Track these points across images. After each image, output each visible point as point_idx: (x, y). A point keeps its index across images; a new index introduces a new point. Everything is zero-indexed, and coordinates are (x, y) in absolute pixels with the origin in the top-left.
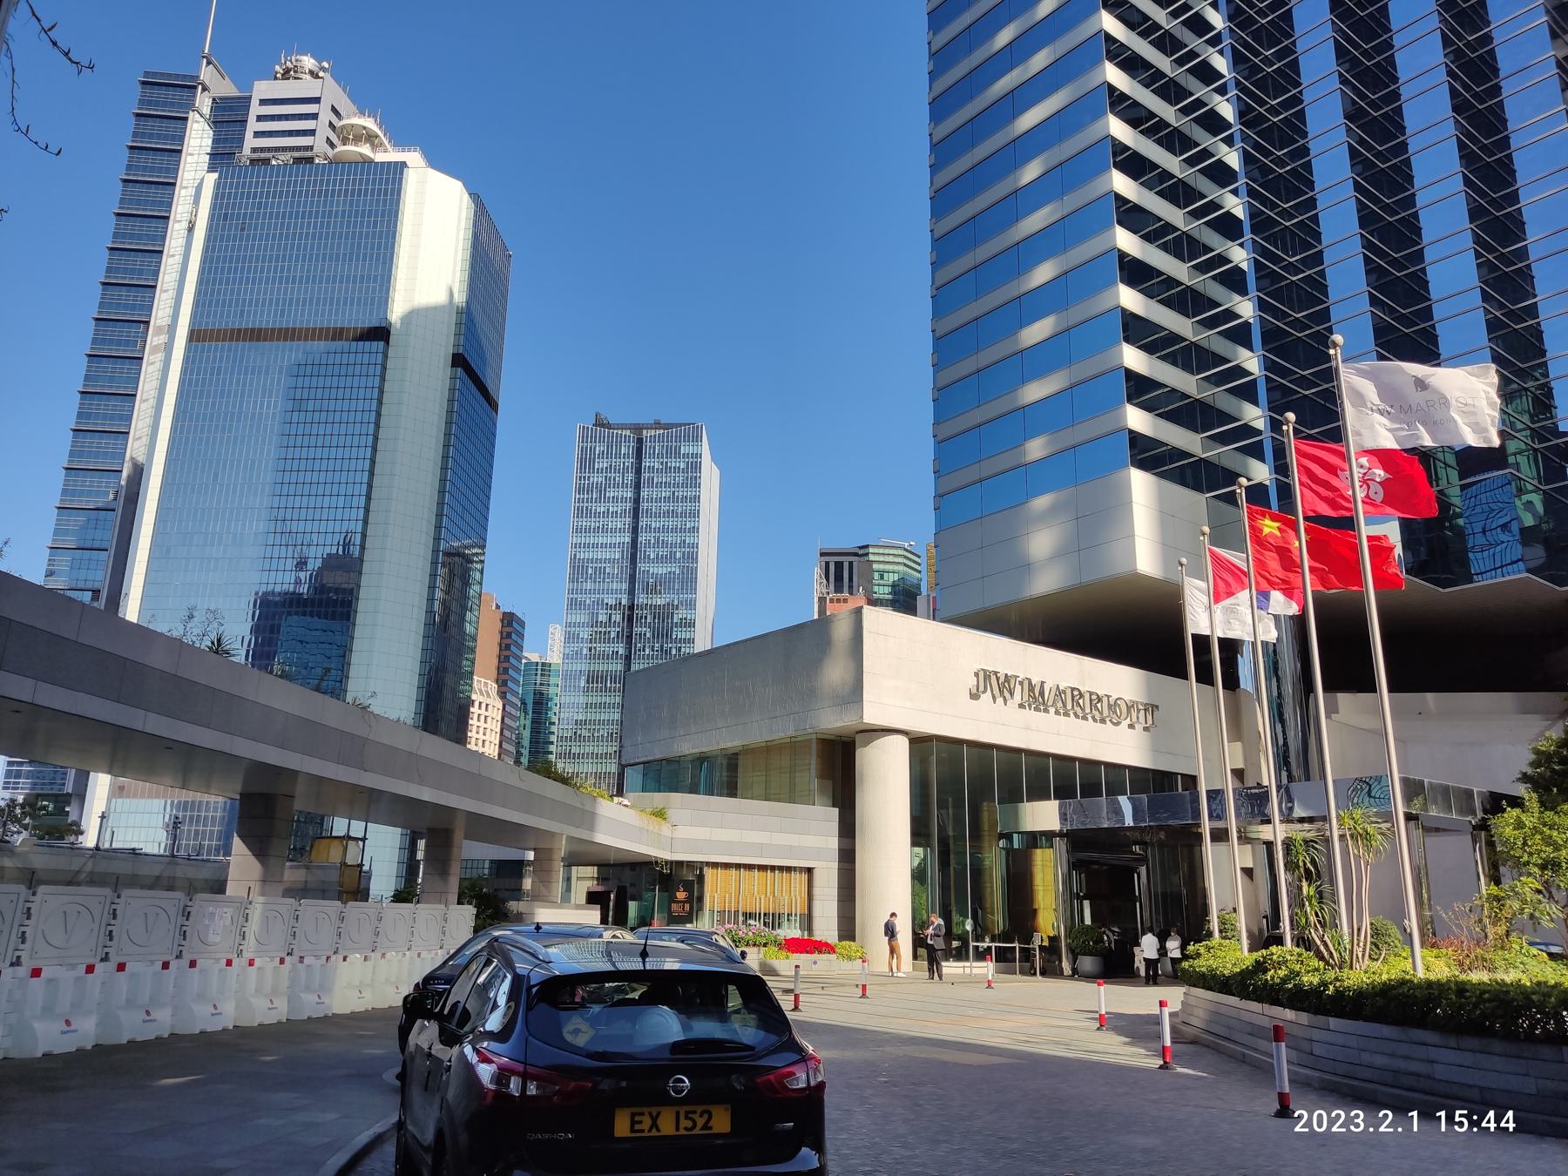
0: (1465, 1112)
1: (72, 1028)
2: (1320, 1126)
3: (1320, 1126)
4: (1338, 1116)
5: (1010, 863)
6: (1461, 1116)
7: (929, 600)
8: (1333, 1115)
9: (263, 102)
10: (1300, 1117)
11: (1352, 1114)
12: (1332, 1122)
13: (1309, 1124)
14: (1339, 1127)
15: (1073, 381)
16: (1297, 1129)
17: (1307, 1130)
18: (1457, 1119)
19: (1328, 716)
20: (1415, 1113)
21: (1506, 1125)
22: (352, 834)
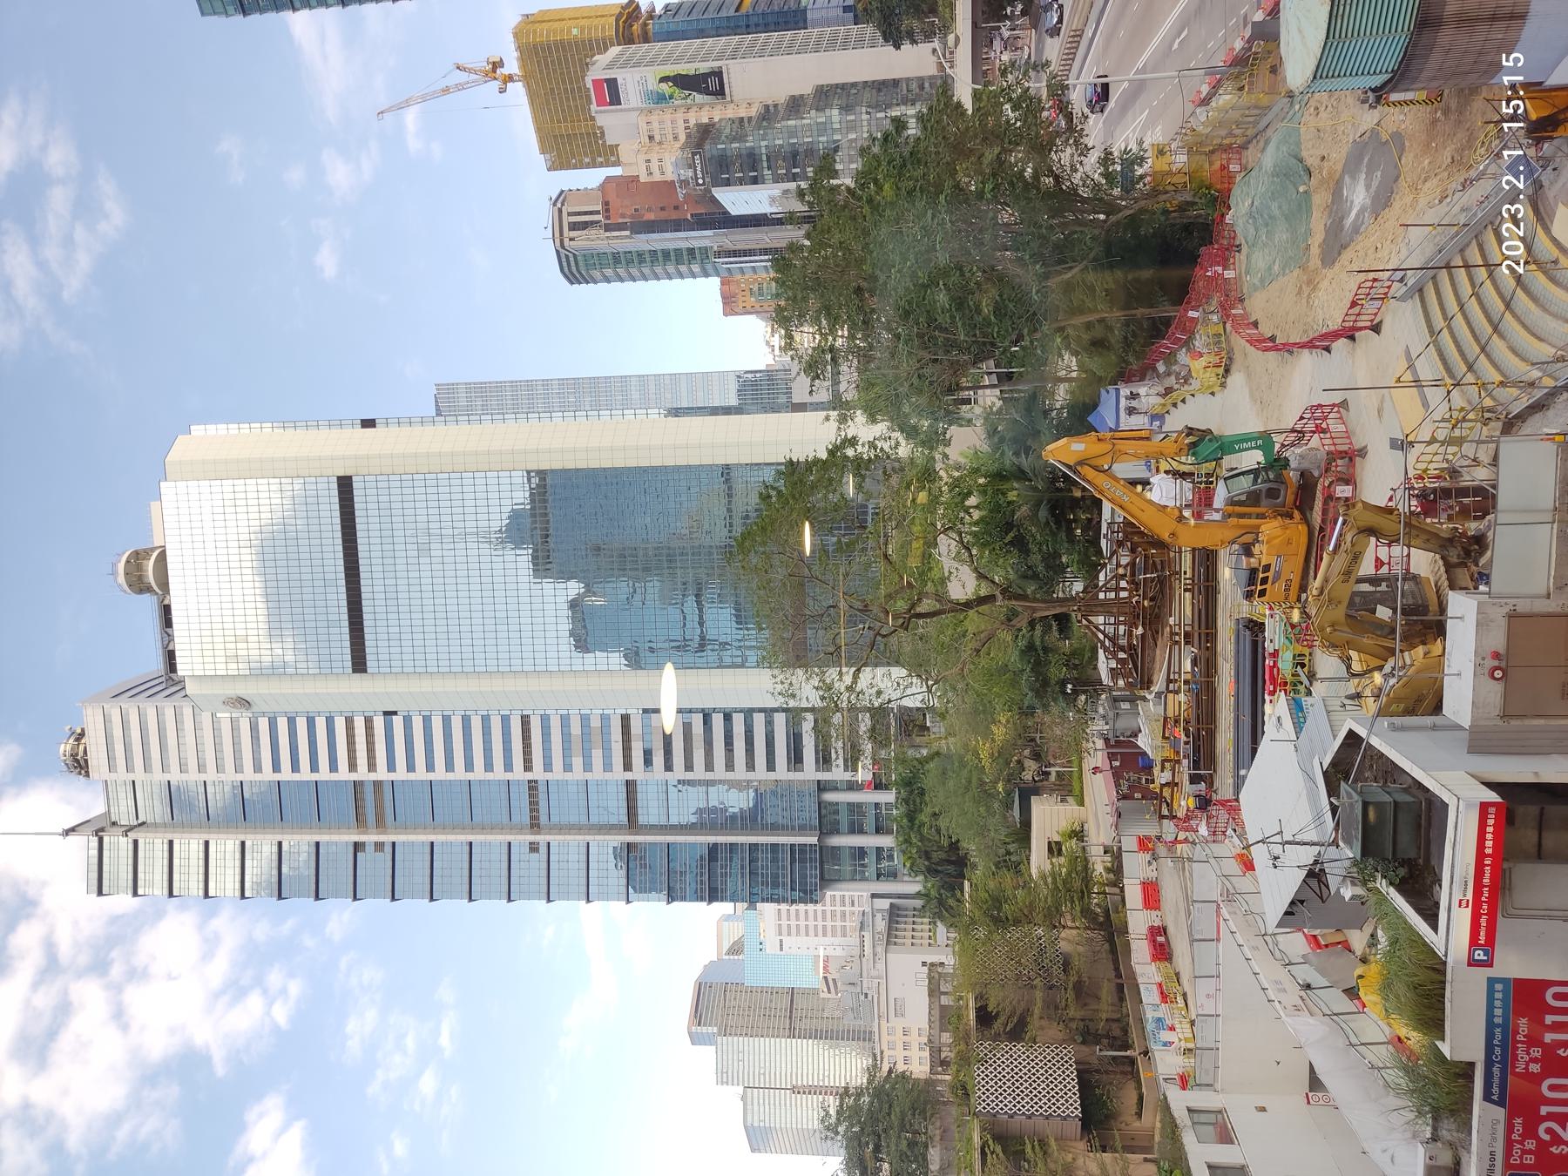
0: (1504, 55)
4: (1508, 229)
6: (1507, 60)
11: (1507, 235)
14: (1519, 230)
18: (1511, 64)
22: (1475, 445)
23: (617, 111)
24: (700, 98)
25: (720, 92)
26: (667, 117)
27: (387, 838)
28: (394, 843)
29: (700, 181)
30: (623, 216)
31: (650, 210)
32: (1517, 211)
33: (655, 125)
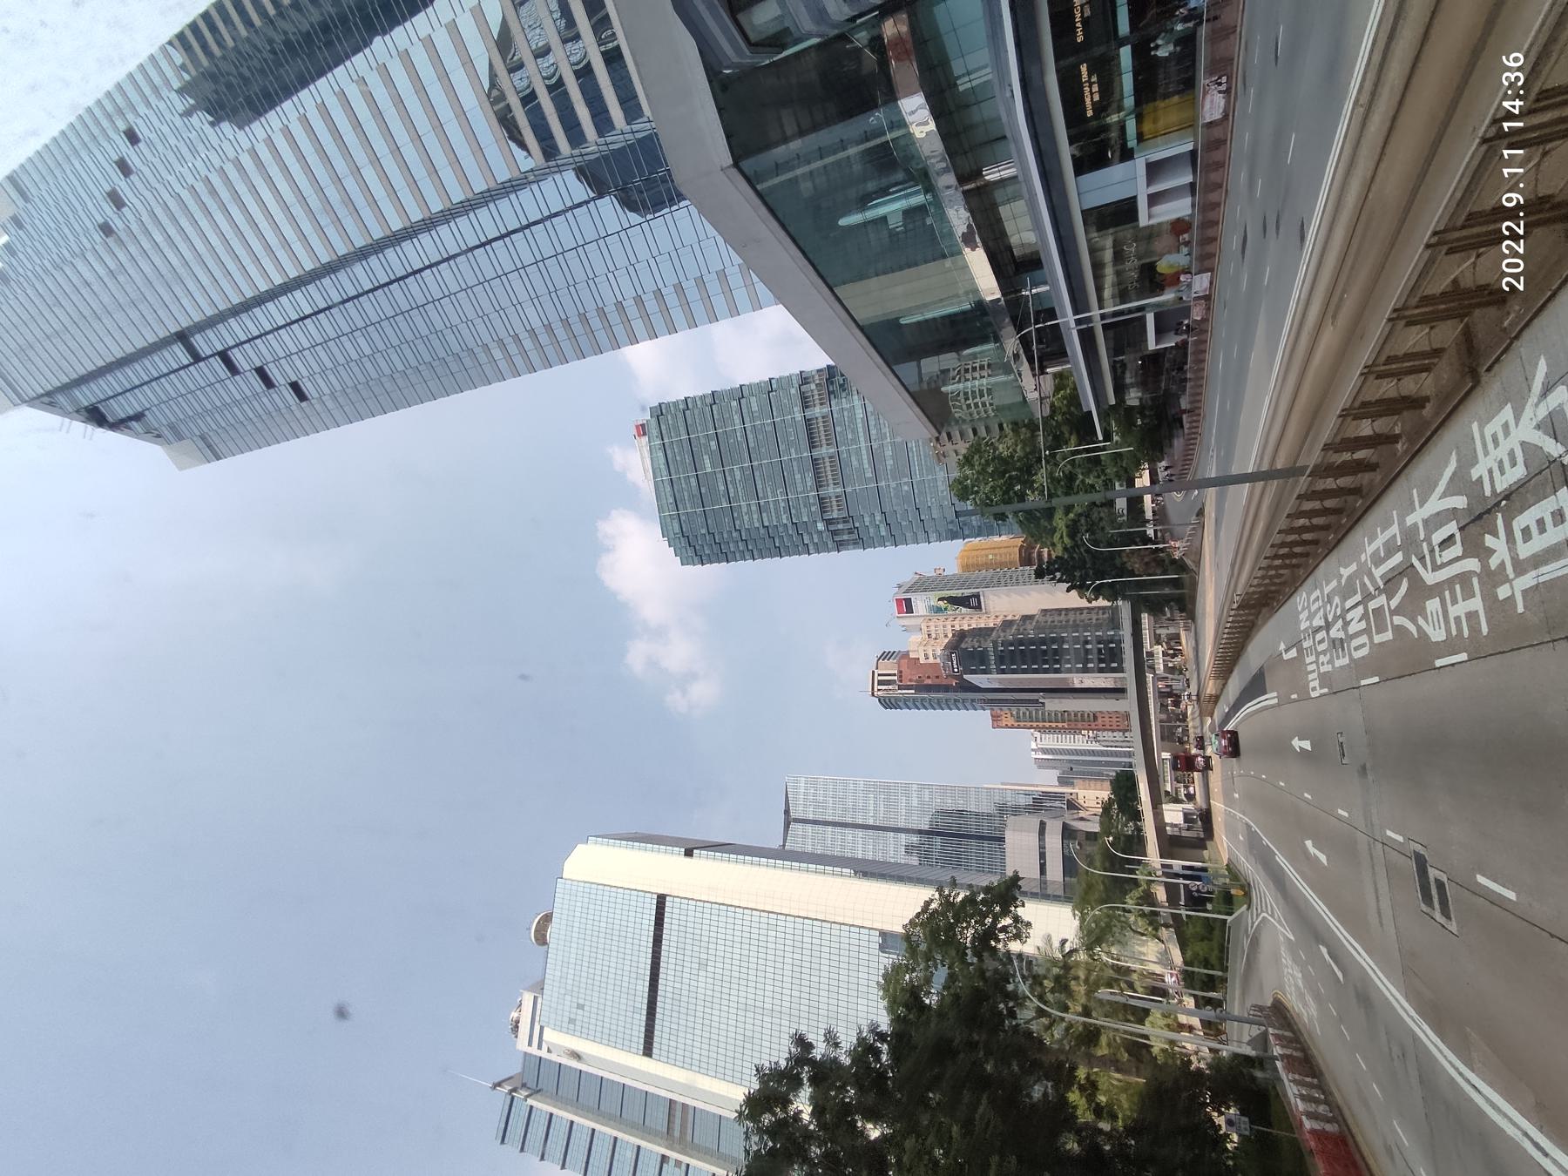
0: (1504, 58)
1: (1069, 765)
2: (1518, 266)
3: (1518, 266)
4: (1508, 247)
5: (1111, 20)
8: (1507, 252)
9: (530, 1044)
10: (1508, 284)
12: (1516, 254)
13: (1516, 277)
16: (1521, 288)
17: (1522, 278)
20: (1506, 171)
21: (1517, 108)
24: (964, 610)
25: (979, 607)
26: (940, 623)
27: (685, 1159)
28: (688, 1165)
30: (910, 680)
31: (929, 677)
33: (933, 628)
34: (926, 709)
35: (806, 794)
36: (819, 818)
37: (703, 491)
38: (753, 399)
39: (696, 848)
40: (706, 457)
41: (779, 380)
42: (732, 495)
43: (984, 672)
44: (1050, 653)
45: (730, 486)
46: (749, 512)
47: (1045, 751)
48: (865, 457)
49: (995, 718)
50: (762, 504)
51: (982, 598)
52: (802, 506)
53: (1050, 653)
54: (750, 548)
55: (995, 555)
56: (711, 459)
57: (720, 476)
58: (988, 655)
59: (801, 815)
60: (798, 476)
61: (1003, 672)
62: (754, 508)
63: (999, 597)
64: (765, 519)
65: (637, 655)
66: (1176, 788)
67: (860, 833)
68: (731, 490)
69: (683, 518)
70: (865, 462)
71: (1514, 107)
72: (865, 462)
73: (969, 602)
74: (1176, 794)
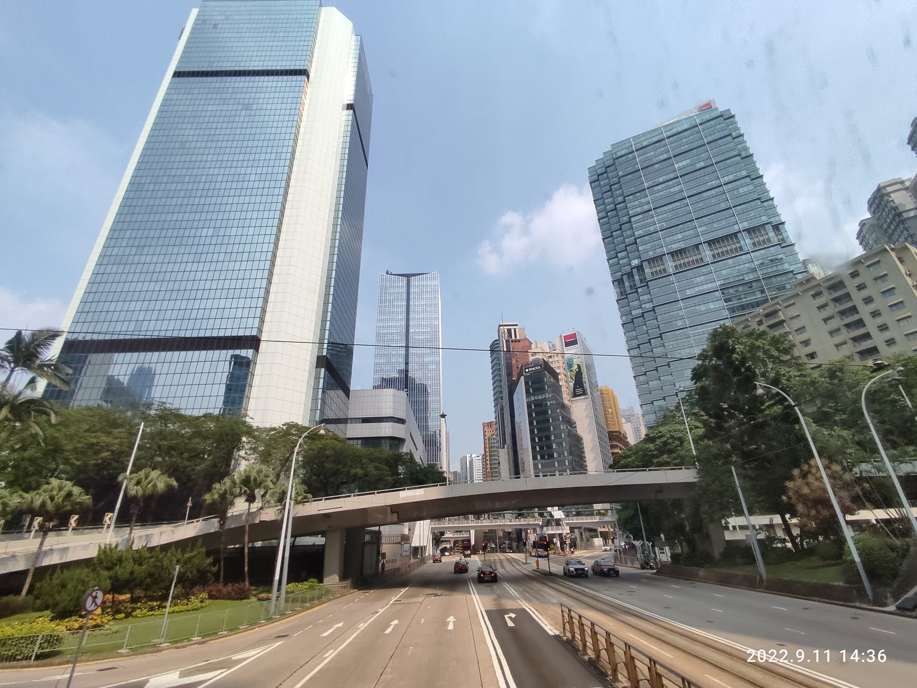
0: (883, 650)
4: (784, 653)
7: (561, 338)
8: (781, 652)
11: (868, 652)
15: (181, 70)
19: (175, 587)
23: (562, 345)
24: (572, 384)
25: (575, 395)
29: (527, 370)
31: (517, 361)
32: (871, 658)
33: (556, 359)
34: (493, 384)
35: (427, 286)
36: (412, 296)
37: (656, 166)
38: (751, 187)
39: (354, 111)
40: (688, 161)
41: (773, 207)
42: (656, 188)
43: (527, 392)
44: (541, 443)
45: (663, 185)
46: (641, 205)
47: (471, 462)
48: (705, 287)
49: (490, 424)
50: (651, 213)
51: (583, 397)
52: (652, 244)
53: (541, 443)
54: (609, 214)
55: (612, 414)
56: (687, 165)
57: (672, 176)
58: (541, 394)
59: (412, 283)
60: (680, 236)
61: (529, 406)
62: (646, 207)
63: (585, 409)
64: (637, 218)
65: (511, 218)
66: (449, 541)
67: (403, 323)
68: (660, 187)
69: (630, 156)
70: (701, 288)
71: (854, 656)
72: (701, 288)
73: (579, 388)
74: (445, 541)
